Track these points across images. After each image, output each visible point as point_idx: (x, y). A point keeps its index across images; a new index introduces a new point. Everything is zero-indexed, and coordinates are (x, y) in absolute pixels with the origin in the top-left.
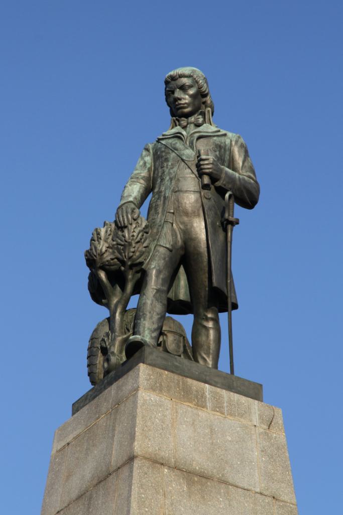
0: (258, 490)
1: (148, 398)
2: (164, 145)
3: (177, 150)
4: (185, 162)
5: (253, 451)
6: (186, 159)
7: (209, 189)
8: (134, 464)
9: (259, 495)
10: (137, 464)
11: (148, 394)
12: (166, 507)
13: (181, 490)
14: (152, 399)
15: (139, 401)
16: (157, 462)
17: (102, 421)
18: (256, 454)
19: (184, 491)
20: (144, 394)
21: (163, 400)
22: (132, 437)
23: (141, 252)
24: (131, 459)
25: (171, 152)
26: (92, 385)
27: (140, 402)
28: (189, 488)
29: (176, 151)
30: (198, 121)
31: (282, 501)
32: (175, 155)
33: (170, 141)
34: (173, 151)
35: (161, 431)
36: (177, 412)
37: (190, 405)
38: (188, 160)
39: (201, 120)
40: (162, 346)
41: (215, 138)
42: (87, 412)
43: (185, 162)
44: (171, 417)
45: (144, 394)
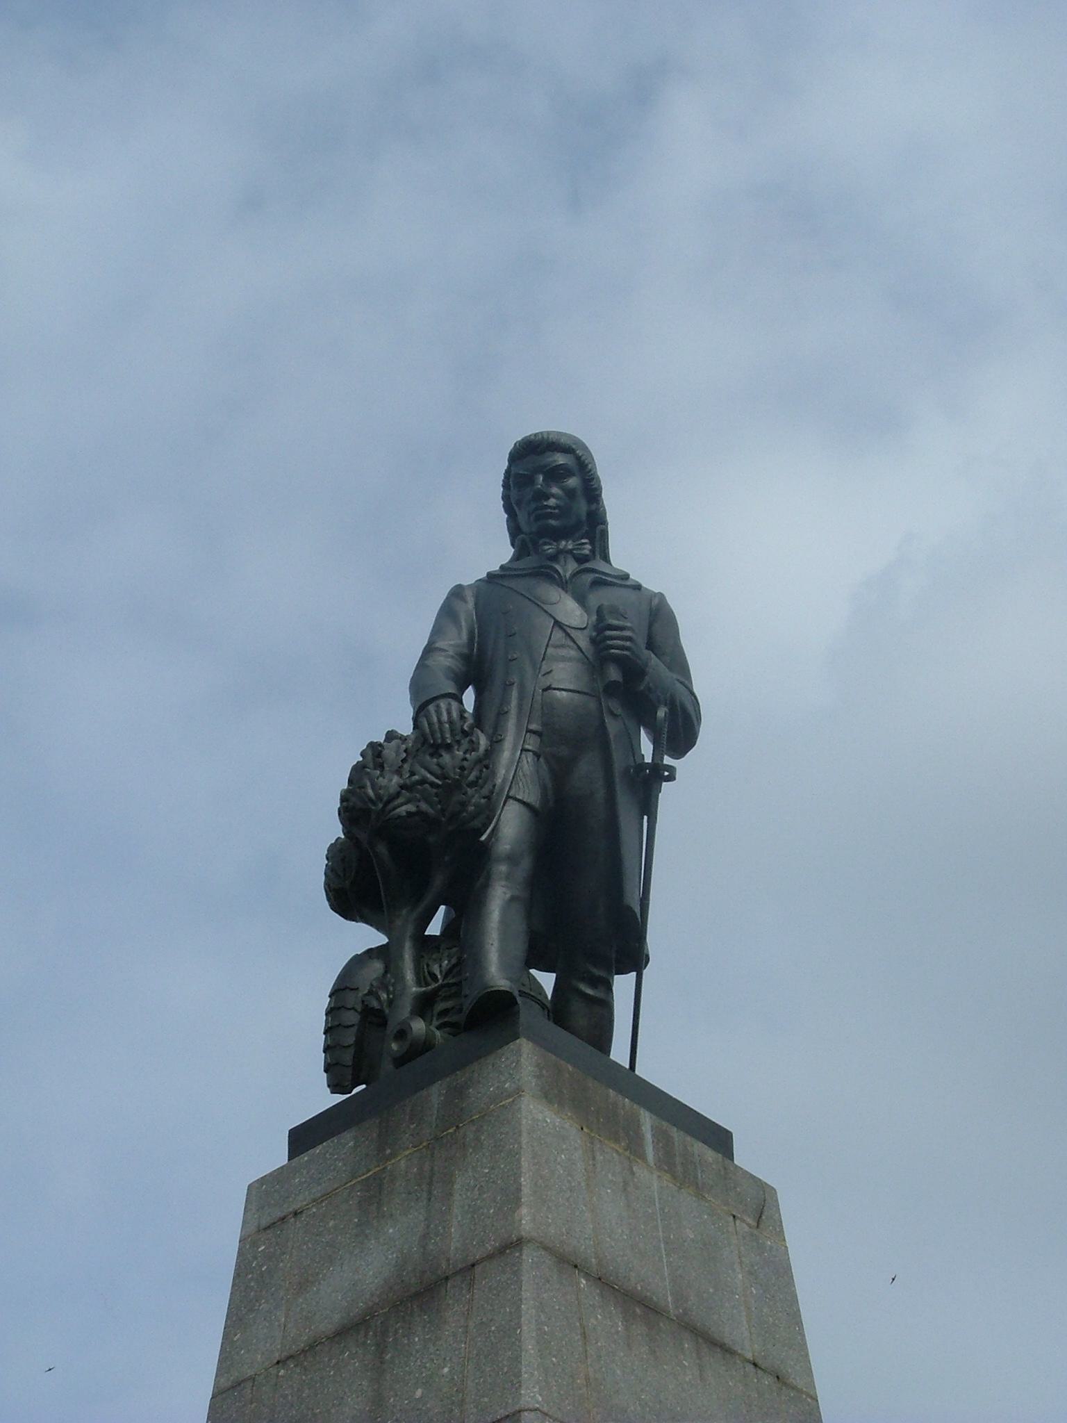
0: (749, 1356)
1: (540, 1117)
4: (565, 631)
5: (734, 1270)
8: (524, 1257)
9: (750, 1368)
10: (529, 1256)
12: (589, 1361)
13: (613, 1330)
15: (524, 1121)
16: (569, 1263)
17: (403, 1162)
18: (740, 1276)
19: (618, 1332)
21: (567, 1126)
22: (514, 1200)
23: (476, 806)
24: (512, 1246)
26: (335, 1087)
27: (525, 1123)
28: (627, 1328)
29: (435, 719)
35: (568, 1194)
36: (594, 1159)
37: (616, 1147)
42: (351, 1144)
43: (565, 631)
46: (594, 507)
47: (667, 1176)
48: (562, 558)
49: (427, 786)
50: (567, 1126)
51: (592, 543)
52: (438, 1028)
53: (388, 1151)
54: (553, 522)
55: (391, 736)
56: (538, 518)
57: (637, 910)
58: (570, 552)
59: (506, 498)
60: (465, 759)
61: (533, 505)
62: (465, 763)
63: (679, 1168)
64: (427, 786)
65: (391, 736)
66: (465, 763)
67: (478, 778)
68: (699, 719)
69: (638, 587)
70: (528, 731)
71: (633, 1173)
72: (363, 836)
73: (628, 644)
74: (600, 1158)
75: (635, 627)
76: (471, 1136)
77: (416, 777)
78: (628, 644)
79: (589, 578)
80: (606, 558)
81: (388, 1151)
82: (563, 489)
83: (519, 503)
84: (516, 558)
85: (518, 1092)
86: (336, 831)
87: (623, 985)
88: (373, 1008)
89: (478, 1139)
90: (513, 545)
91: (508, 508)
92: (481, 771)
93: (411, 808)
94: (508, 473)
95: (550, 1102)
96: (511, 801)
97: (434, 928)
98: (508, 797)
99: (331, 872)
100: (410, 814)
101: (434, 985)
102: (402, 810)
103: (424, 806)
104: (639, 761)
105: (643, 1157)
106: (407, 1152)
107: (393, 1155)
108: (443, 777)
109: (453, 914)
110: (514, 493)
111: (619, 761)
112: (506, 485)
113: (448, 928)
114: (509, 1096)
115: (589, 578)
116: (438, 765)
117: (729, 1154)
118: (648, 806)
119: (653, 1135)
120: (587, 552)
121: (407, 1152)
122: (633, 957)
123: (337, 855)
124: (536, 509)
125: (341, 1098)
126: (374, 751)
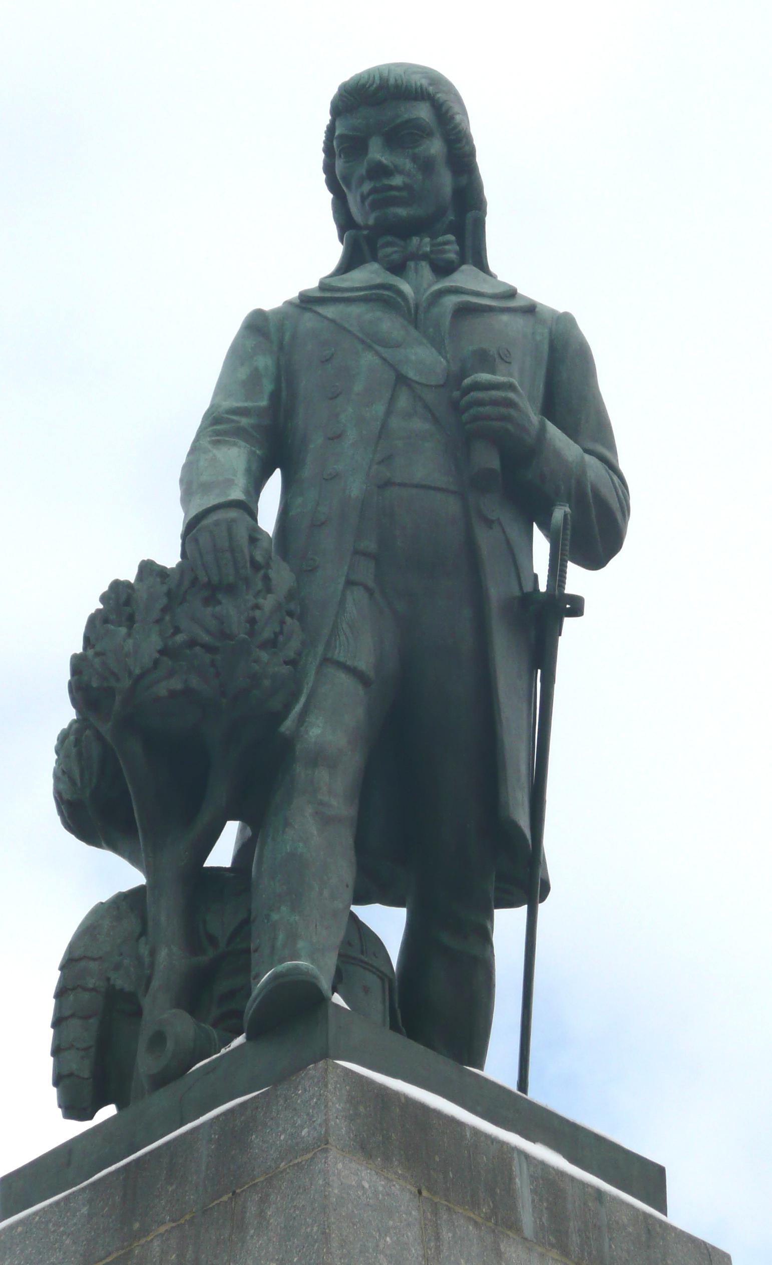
2: (333, 321)
3: (385, 344)
6: (416, 378)
7: (402, 136)
11: (353, 1165)
14: (367, 1186)
20: (340, 1166)
25: (360, 347)
26: (75, 1106)
29: (379, 348)
30: (444, 252)
31: (402, 485)
32: (377, 360)
33: (355, 310)
34: (369, 347)
36: (438, 1238)
38: (423, 381)
39: (451, 253)
40: (519, 1093)
41: (505, 318)
42: (85, 1210)
44: (420, 1253)
45: (340, 1166)
46: (464, 180)
47: (554, 1254)
48: (412, 264)
49: (198, 649)
50: (396, 1189)
51: (460, 241)
52: (215, 1025)
53: (137, 1226)
54: (402, 212)
55: (147, 569)
56: (374, 206)
57: (524, 823)
58: (425, 257)
59: (329, 168)
60: (257, 607)
61: (367, 187)
62: (257, 613)
63: (575, 1239)
64: (198, 649)
65: (147, 569)
66: (257, 613)
67: (276, 635)
68: (625, 510)
69: (531, 309)
70: (356, 552)
71: (499, 1254)
72: (106, 729)
73: (503, 410)
74: (446, 1235)
75: (519, 382)
76: (252, 1209)
77: (180, 638)
78: (503, 410)
79: (451, 301)
80: (481, 263)
81: (137, 1226)
82: (414, 158)
83: (347, 179)
84: (348, 264)
85: (322, 1143)
86: (67, 714)
87: (507, 923)
88: (122, 990)
89: (261, 1214)
90: (341, 240)
91: (333, 184)
92: (283, 622)
93: (176, 684)
94: (331, 131)
95: (370, 1156)
96: (330, 670)
97: (222, 854)
98: (326, 660)
99: (63, 775)
100: (173, 694)
101: (211, 954)
102: (162, 690)
103: (195, 682)
104: (528, 588)
105: (514, 1225)
106: (162, 1229)
107: (145, 1231)
108: (225, 635)
109: (249, 832)
110: (339, 164)
111: (497, 590)
112: (329, 150)
113: (244, 852)
114: (306, 1150)
115: (451, 301)
116: (214, 616)
117: (658, 1199)
118: (542, 656)
119: (534, 1192)
120: (452, 256)
121: (162, 1229)
122: (526, 883)
123: (73, 747)
124: (373, 191)
125: (77, 1128)
126: (119, 598)
